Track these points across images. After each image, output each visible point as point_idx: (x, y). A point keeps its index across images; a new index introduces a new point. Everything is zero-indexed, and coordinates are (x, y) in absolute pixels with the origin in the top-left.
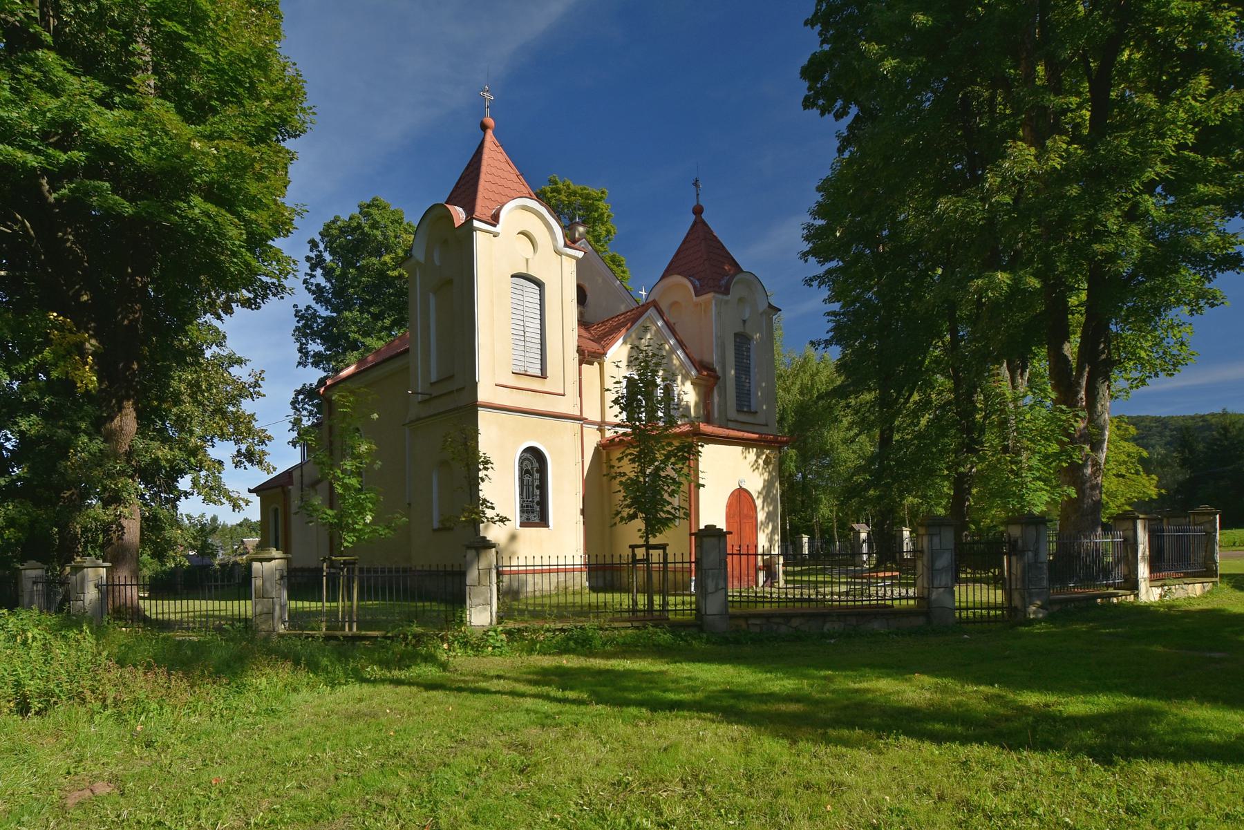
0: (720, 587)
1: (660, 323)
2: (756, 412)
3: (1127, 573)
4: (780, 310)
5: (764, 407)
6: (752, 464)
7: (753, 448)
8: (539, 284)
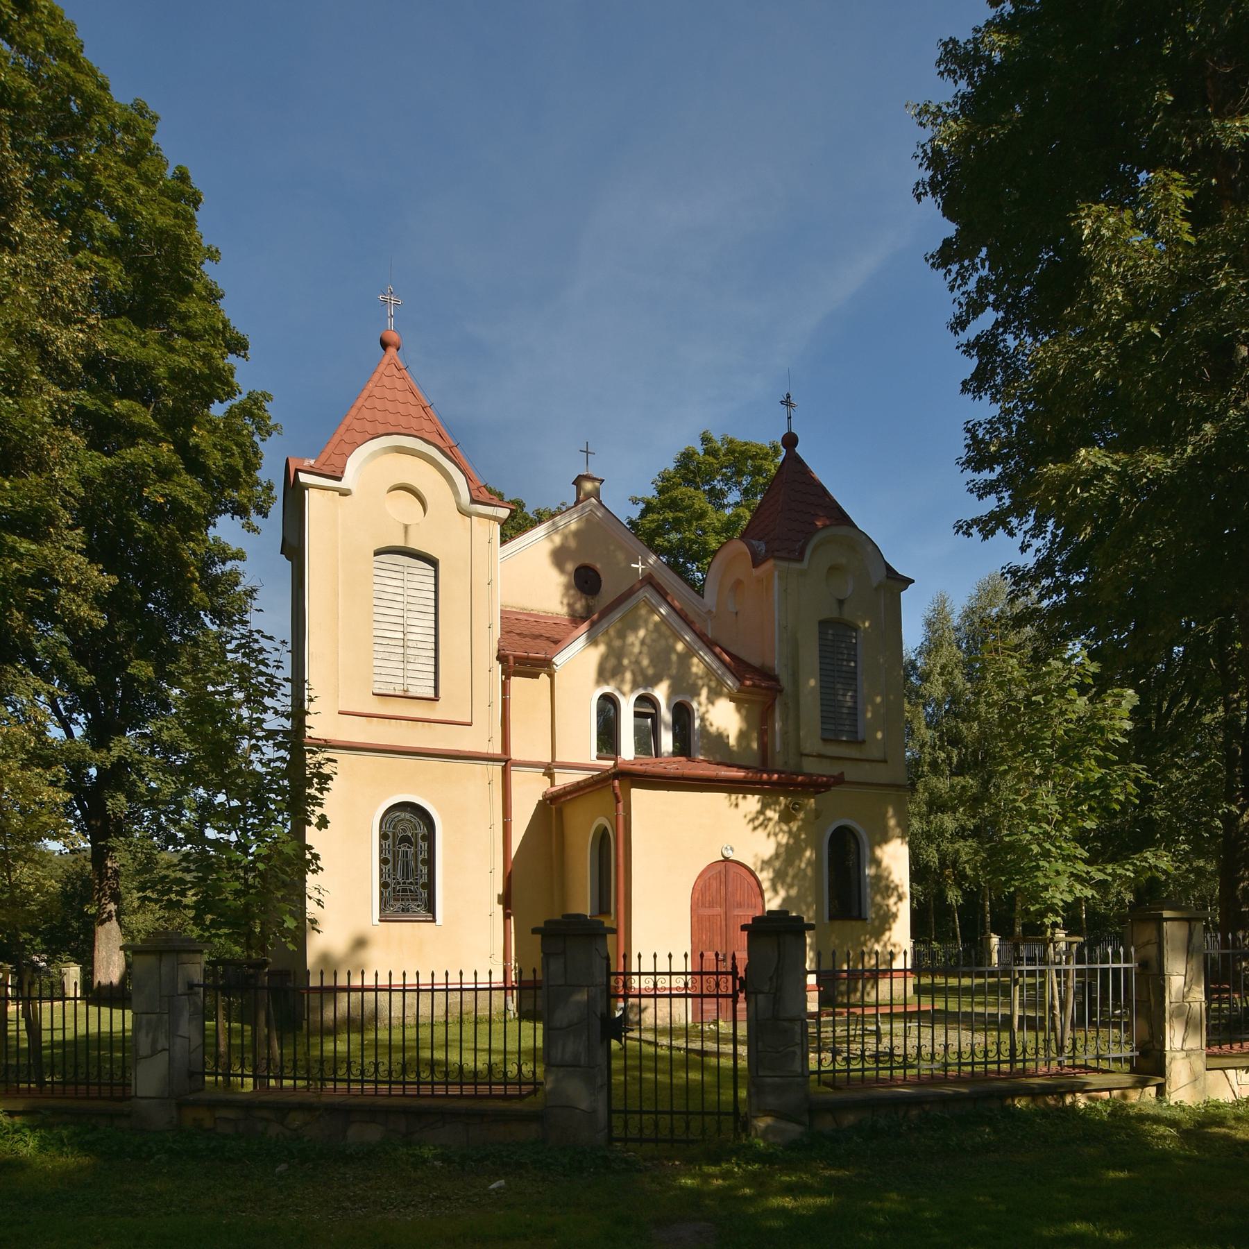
0: (160, 1048)
2: (863, 742)
3: (1147, 1038)
4: (912, 581)
5: (879, 735)
6: (749, 817)
7: (753, 794)
8: (433, 562)
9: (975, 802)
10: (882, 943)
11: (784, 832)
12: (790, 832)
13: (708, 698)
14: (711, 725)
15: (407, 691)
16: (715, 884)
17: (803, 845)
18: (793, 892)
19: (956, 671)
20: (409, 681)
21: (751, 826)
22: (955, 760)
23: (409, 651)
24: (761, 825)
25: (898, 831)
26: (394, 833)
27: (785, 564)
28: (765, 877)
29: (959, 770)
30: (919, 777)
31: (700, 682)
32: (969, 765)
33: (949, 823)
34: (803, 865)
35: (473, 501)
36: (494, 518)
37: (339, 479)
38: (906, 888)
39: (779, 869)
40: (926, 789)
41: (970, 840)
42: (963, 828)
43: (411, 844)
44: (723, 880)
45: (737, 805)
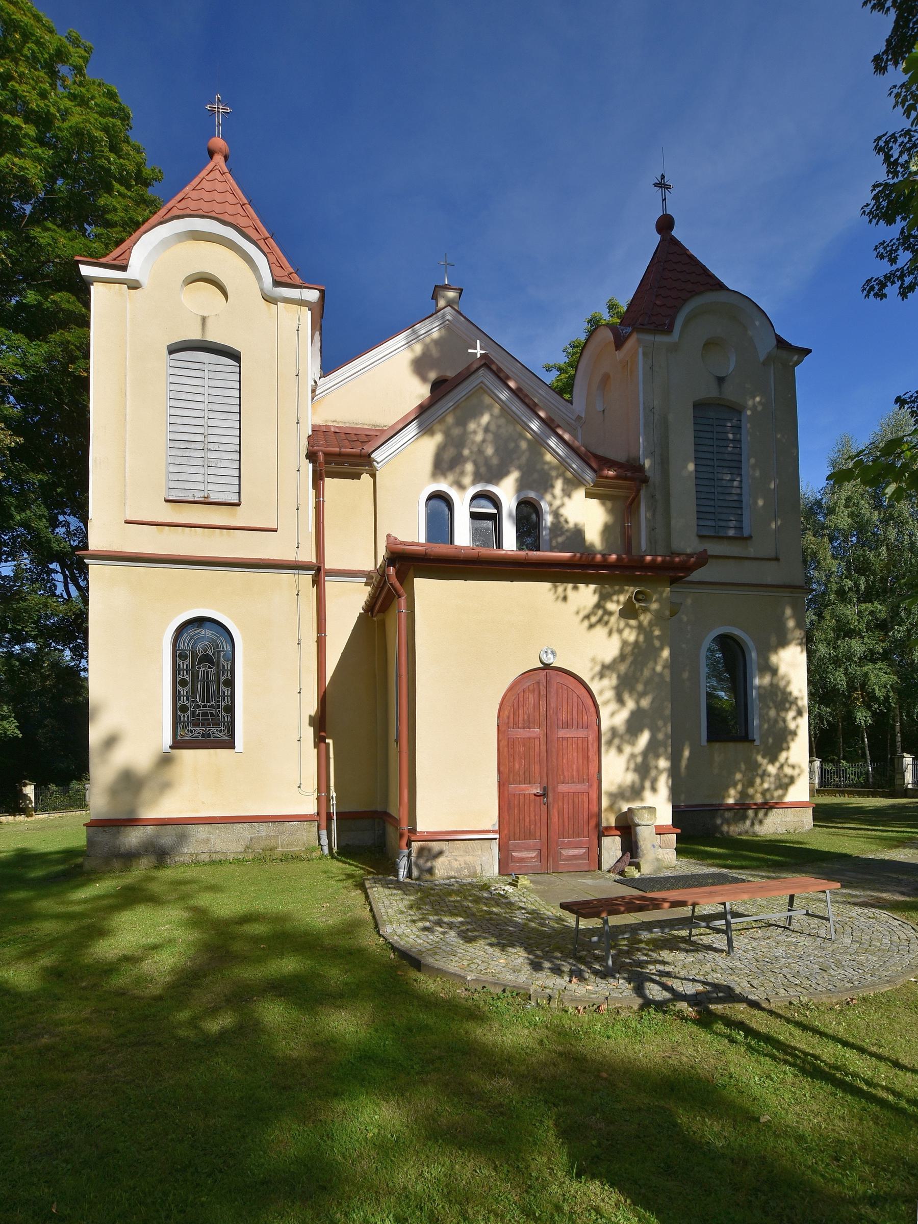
1: (504, 395)
2: (750, 537)
6: (582, 615)
7: (587, 583)
8: (235, 356)
9: (883, 626)
10: (777, 764)
11: (631, 627)
12: (640, 627)
13: (563, 490)
14: (566, 522)
16: (531, 698)
17: (657, 643)
18: (645, 703)
19: (862, 502)
20: (210, 487)
21: (586, 623)
22: (863, 587)
24: (600, 621)
26: (193, 652)
27: (648, 338)
28: (604, 689)
29: (867, 597)
30: (826, 606)
31: (554, 473)
32: (877, 592)
33: (857, 647)
34: (659, 668)
35: (277, 283)
36: (301, 303)
37: (124, 268)
38: (804, 702)
39: (626, 674)
40: (833, 616)
41: (879, 663)
42: (871, 651)
43: (212, 662)
44: (543, 692)
45: (565, 599)
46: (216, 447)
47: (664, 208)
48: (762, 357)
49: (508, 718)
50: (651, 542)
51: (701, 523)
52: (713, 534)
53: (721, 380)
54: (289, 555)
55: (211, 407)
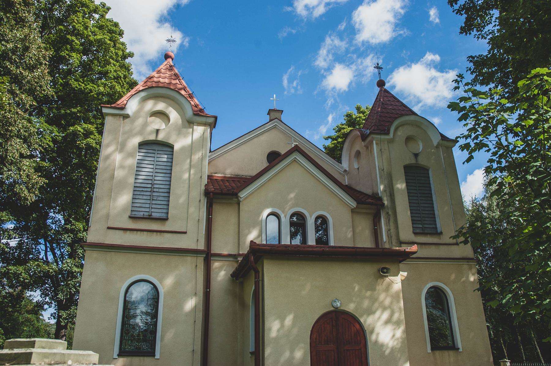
15: (151, 215)
20: (153, 210)
23: (155, 194)
25: (149, 94)
46: (157, 190)
47: (380, 77)
48: (435, 144)
49: (316, 339)
50: (388, 237)
51: (415, 226)
52: (422, 232)
53: (416, 155)
54: (193, 246)
55: (157, 170)
